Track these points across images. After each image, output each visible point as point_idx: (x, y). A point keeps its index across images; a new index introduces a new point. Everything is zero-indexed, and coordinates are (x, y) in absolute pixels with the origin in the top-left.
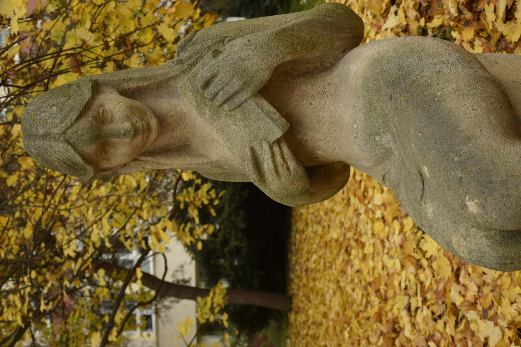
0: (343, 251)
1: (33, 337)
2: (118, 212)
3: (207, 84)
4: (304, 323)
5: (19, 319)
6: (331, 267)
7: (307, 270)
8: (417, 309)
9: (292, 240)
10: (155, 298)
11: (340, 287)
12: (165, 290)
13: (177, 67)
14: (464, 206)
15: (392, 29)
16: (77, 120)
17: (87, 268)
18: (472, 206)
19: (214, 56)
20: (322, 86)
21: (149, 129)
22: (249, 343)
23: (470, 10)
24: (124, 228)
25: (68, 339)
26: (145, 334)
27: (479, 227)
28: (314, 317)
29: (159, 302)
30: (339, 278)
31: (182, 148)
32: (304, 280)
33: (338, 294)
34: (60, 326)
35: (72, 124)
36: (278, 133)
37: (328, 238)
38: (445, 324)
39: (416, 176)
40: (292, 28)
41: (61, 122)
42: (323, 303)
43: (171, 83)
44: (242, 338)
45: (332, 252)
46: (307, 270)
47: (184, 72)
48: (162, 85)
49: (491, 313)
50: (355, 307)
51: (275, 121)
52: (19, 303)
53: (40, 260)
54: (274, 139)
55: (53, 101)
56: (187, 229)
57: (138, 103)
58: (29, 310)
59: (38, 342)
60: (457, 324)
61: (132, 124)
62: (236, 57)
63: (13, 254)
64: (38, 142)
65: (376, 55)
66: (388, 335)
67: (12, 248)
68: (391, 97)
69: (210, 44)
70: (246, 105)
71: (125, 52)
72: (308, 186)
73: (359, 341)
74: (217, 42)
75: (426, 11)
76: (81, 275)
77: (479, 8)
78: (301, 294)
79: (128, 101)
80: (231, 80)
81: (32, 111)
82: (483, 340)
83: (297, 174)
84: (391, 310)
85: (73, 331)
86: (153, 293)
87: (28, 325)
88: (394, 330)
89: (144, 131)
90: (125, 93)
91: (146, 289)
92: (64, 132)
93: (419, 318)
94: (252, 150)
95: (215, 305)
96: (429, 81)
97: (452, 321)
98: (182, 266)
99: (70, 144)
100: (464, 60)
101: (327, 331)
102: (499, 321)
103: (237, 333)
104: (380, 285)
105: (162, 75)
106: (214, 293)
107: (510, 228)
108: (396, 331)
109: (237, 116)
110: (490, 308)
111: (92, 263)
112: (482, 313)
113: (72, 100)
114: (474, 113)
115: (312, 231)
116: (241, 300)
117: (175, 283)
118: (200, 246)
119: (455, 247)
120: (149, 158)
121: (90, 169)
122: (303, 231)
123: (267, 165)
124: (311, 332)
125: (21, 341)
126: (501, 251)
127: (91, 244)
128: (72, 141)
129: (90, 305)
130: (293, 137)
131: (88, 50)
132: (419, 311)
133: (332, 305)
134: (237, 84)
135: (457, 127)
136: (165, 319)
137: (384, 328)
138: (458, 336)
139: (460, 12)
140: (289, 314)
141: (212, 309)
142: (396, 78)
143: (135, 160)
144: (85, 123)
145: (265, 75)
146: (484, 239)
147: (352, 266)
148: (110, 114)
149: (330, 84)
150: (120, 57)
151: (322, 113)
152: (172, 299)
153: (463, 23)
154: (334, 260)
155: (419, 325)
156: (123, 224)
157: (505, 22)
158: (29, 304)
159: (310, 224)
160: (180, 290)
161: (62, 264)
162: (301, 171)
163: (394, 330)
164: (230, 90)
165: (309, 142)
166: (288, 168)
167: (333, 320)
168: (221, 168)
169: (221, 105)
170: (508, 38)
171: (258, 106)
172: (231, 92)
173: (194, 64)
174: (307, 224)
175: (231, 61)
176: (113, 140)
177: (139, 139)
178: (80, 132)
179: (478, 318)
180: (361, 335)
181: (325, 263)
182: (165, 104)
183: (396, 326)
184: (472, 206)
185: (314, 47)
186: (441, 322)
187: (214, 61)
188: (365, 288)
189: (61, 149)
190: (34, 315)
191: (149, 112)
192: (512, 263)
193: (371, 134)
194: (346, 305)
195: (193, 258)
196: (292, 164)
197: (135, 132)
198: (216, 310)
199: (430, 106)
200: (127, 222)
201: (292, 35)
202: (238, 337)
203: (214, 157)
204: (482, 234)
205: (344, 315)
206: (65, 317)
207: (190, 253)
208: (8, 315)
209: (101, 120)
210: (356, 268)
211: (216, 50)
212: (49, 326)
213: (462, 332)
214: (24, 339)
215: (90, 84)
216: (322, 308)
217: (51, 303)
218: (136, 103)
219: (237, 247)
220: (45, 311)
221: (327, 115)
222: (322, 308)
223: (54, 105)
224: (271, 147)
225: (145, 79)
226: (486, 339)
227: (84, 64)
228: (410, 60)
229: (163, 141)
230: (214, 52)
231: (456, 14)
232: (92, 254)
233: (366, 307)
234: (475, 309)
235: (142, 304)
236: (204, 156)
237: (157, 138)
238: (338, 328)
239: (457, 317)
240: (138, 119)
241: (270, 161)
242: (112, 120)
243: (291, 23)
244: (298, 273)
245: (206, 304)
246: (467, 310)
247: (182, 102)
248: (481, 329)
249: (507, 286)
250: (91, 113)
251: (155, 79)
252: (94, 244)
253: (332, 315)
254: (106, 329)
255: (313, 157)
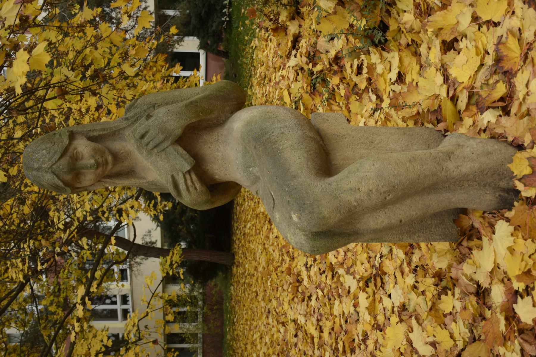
0: (267, 222)
1: (32, 288)
2: (96, 194)
3: (142, 137)
4: (243, 274)
5: (21, 276)
6: (260, 233)
7: (244, 234)
8: (311, 266)
9: (235, 210)
10: (127, 257)
11: (265, 249)
12: (137, 250)
13: (125, 122)
14: (291, 217)
15: (293, 67)
16: (59, 159)
17: (74, 236)
18: (295, 218)
19: (147, 119)
20: (217, 136)
21: (107, 162)
22: (203, 289)
23: (337, 64)
24: (102, 206)
25: (59, 290)
26: (120, 284)
27: (298, 228)
28: (249, 270)
29: (132, 259)
30: (265, 242)
31: (130, 173)
32: (243, 241)
33: (264, 253)
34: (53, 280)
35: (56, 162)
36: (188, 167)
37: (258, 211)
38: (326, 277)
39: (270, 195)
40: (196, 101)
41: (49, 160)
42: (255, 259)
43: (121, 132)
44: (197, 285)
45: (260, 222)
46: (244, 234)
47: (129, 126)
48: (115, 133)
49: (352, 270)
50: (274, 264)
51: (186, 160)
52: (20, 265)
53: (37, 229)
54: (186, 170)
55: (44, 146)
56: (151, 205)
57: (100, 145)
58: (29, 267)
59: (36, 292)
60: (333, 277)
61: (95, 160)
62: (161, 120)
63: (15, 225)
64: (34, 173)
65: (249, 118)
66: (293, 284)
67: (14, 221)
68: (255, 147)
69: (145, 109)
70: (168, 149)
71: (98, 83)
72: (210, 198)
73: (277, 288)
74: (151, 107)
75: (313, 58)
76: (68, 242)
77: (342, 64)
78: (240, 252)
79: (93, 144)
80: (157, 135)
81: (30, 152)
82: (347, 288)
83: (202, 191)
84: (296, 266)
85: (64, 283)
86: (126, 252)
87: (28, 280)
88: (298, 281)
89: (103, 165)
90: (92, 139)
91: (121, 250)
92: (51, 167)
93: (312, 273)
94: (173, 177)
95: (174, 263)
96: (276, 139)
97: (330, 276)
98: (150, 232)
99: (55, 174)
100: (299, 125)
101: (257, 281)
102: (356, 275)
103: (192, 282)
104: (290, 248)
105: (115, 127)
106: (173, 254)
107: (314, 231)
108: (300, 282)
109: (163, 156)
110: (351, 266)
111: (77, 233)
112: (346, 270)
113: (56, 145)
114: (299, 161)
115: (248, 205)
116: (195, 257)
117: (144, 244)
118: (161, 217)
119: (290, 240)
120: (108, 180)
121: (68, 189)
122: (242, 205)
123: (182, 186)
124: (247, 281)
125: (22, 292)
126: (311, 243)
127: (76, 219)
128: (56, 173)
129: (77, 263)
130: (198, 167)
131: (70, 83)
132: (312, 267)
133: (261, 261)
134: (161, 137)
135: (289, 169)
136: (136, 272)
137: (290, 279)
138: (334, 286)
139: (331, 65)
140: (232, 267)
141: (171, 265)
142: (259, 136)
143: (99, 181)
144: (65, 161)
145: (179, 132)
146: (302, 236)
147: (273, 233)
148: (81, 154)
149: (222, 135)
150: (93, 88)
151: (217, 153)
152: (143, 257)
153: (332, 72)
154: (262, 228)
155: (312, 277)
156: (100, 204)
157: (357, 76)
158: (29, 263)
159: (246, 200)
160: (148, 250)
161: (54, 233)
162: (204, 189)
163: (298, 281)
164: (157, 141)
165: (210, 170)
166: (196, 188)
167: (261, 272)
168: (155, 185)
169: (152, 149)
170: (359, 86)
171: (175, 150)
172: (158, 142)
173: (136, 121)
174: (244, 199)
175: (157, 123)
176: (83, 171)
177: (100, 170)
178: (61, 167)
179: (345, 273)
180: (279, 283)
181: (256, 230)
182: (117, 146)
183: (299, 278)
184: (295, 218)
185: (211, 112)
186: (324, 276)
187: (147, 123)
188: (281, 250)
189: (49, 178)
190: (33, 274)
191: (107, 152)
192: (318, 250)
193: (247, 167)
194: (269, 261)
195: (158, 226)
196: (198, 185)
197: (98, 165)
198: (175, 266)
199: (275, 156)
200: (104, 202)
201: (196, 106)
202: (193, 285)
203: (150, 179)
204: (302, 233)
205: (268, 269)
206: (57, 273)
207: (155, 222)
208: (12, 273)
209: (75, 158)
210: (275, 234)
211: (149, 115)
212: (44, 280)
213: (335, 283)
214: (24, 291)
215: (67, 134)
216: (254, 263)
217: (46, 264)
218: (98, 146)
219: (192, 216)
220: (41, 270)
221: (220, 154)
222: (254, 263)
223: (44, 149)
224: (184, 175)
225: (104, 130)
226: (349, 287)
227: (67, 93)
228: (267, 124)
229: (117, 169)
230: (147, 116)
231: (328, 66)
232: (77, 226)
233: (282, 264)
234: (343, 267)
235: (118, 263)
236: (144, 178)
237: (112, 168)
238: (264, 279)
239: (333, 273)
240: (99, 157)
241: (184, 184)
242: (82, 158)
243: (196, 97)
244: (239, 236)
245: (166, 261)
246: (339, 268)
247: (127, 145)
248: (346, 281)
249: (359, 252)
250: (69, 154)
251: (110, 130)
252: (78, 219)
253: (260, 269)
254: (88, 283)
255: (212, 179)
